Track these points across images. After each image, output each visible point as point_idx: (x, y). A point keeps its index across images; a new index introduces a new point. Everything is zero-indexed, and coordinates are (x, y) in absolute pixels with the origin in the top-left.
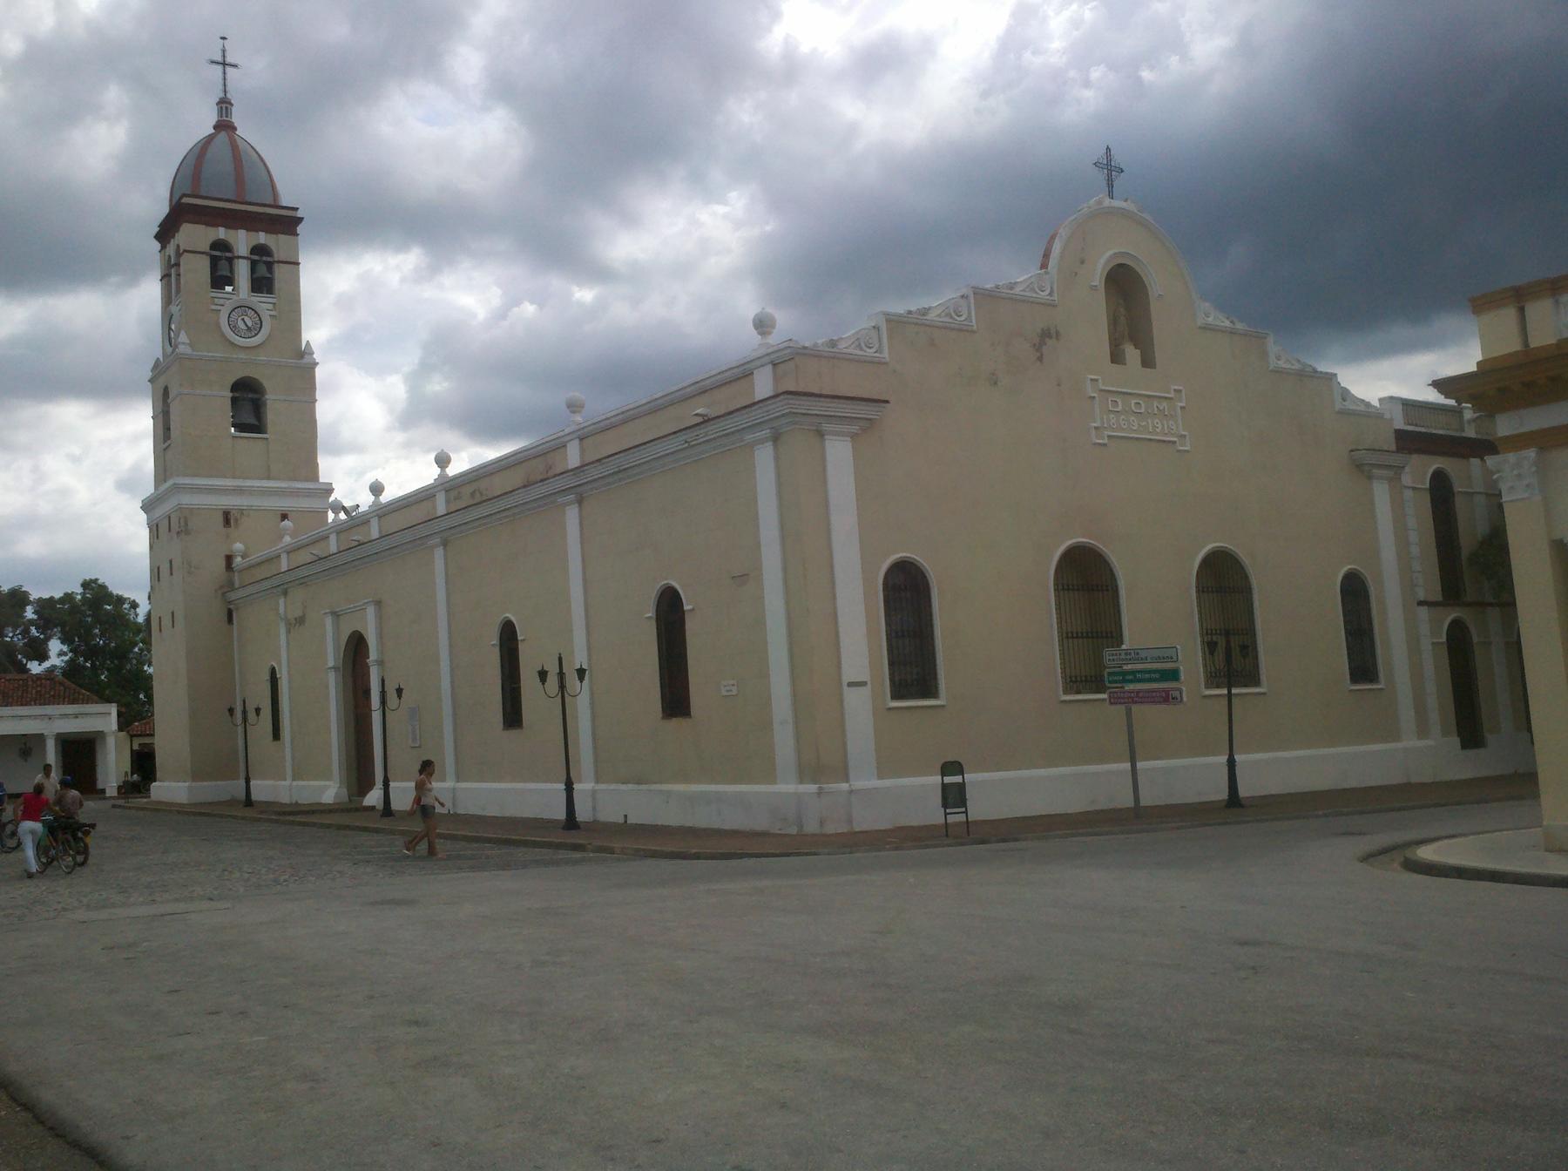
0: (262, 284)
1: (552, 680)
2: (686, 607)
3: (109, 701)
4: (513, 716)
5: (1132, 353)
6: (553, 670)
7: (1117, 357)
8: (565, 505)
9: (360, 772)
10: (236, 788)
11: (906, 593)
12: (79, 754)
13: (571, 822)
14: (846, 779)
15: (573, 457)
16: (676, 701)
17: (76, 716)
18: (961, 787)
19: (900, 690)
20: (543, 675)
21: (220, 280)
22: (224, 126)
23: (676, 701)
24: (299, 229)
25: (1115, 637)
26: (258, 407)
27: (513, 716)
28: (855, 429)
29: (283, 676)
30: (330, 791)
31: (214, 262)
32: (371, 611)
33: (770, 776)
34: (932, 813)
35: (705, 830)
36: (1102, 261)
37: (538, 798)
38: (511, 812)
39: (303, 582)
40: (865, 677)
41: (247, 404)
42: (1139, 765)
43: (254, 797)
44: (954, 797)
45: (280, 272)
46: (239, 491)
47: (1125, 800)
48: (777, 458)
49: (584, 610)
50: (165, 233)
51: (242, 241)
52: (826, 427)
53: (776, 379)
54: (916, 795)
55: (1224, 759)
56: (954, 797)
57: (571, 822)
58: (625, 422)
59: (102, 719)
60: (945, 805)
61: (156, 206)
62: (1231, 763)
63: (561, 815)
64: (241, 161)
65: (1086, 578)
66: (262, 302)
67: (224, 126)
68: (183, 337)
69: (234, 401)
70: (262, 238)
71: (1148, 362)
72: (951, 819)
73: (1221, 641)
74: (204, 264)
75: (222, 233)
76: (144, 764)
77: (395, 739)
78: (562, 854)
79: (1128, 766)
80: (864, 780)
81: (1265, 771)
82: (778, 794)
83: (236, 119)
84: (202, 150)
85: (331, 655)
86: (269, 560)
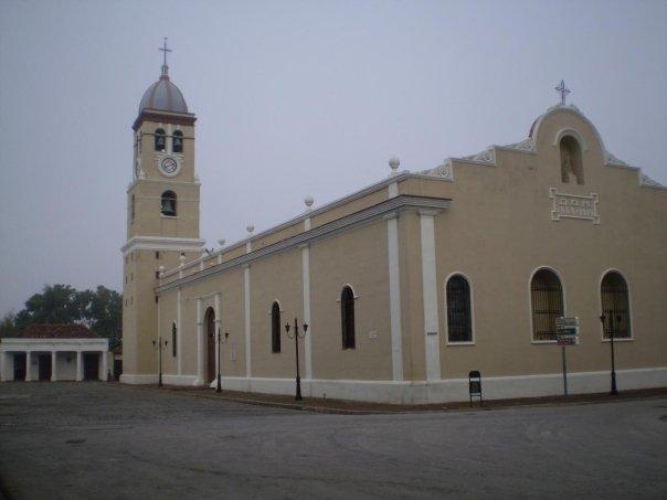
0: (178, 149)
1: (292, 331)
2: (355, 296)
3: (103, 336)
4: (277, 348)
5: (572, 178)
6: (292, 326)
7: (565, 179)
8: (387, 220)
9: (210, 371)
10: (152, 378)
11: (458, 290)
12: (92, 360)
13: (299, 397)
14: (426, 379)
15: (307, 226)
16: (349, 341)
17: (91, 343)
18: (479, 383)
19: (453, 337)
20: (288, 327)
21: (160, 147)
22: (165, 78)
23: (349, 341)
24: (195, 124)
25: (560, 312)
26: (173, 204)
27: (277, 348)
28: (435, 212)
29: (178, 327)
30: (197, 380)
31: (157, 138)
32: (217, 299)
33: (245, 375)
34: (464, 395)
35: (393, 406)
36: (557, 135)
37: (283, 385)
38: (275, 392)
39: (188, 284)
40: (437, 330)
41: (169, 201)
42: (568, 375)
43: (163, 382)
44: (475, 388)
45: (186, 143)
46: (163, 242)
47: (560, 392)
48: (398, 226)
49: (308, 294)
50: (137, 126)
51: (170, 129)
52: (421, 211)
53: (399, 190)
54: (459, 388)
55: (610, 372)
56: (475, 388)
57: (299, 397)
58: (281, 230)
59: (101, 345)
60: (471, 392)
61: (135, 115)
62: (613, 374)
63: (294, 394)
64: (173, 93)
65: (546, 282)
66: (177, 157)
67: (165, 78)
68: (142, 173)
69: (163, 201)
70: (178, 127)
71: (580, 182)
72: (473, 399)
73: (607, 315)
74: (152, 140)
75: (160, 125)
76: (118, 368)
77: (223, 352)
78: (255, 408)
79: (561, 375)
80: (434, 378)
81: (629, 379)
82: (393, 386)
83: (169, 75)
84: (153, 91)
85: (200, 317)
86: (174, 274)
